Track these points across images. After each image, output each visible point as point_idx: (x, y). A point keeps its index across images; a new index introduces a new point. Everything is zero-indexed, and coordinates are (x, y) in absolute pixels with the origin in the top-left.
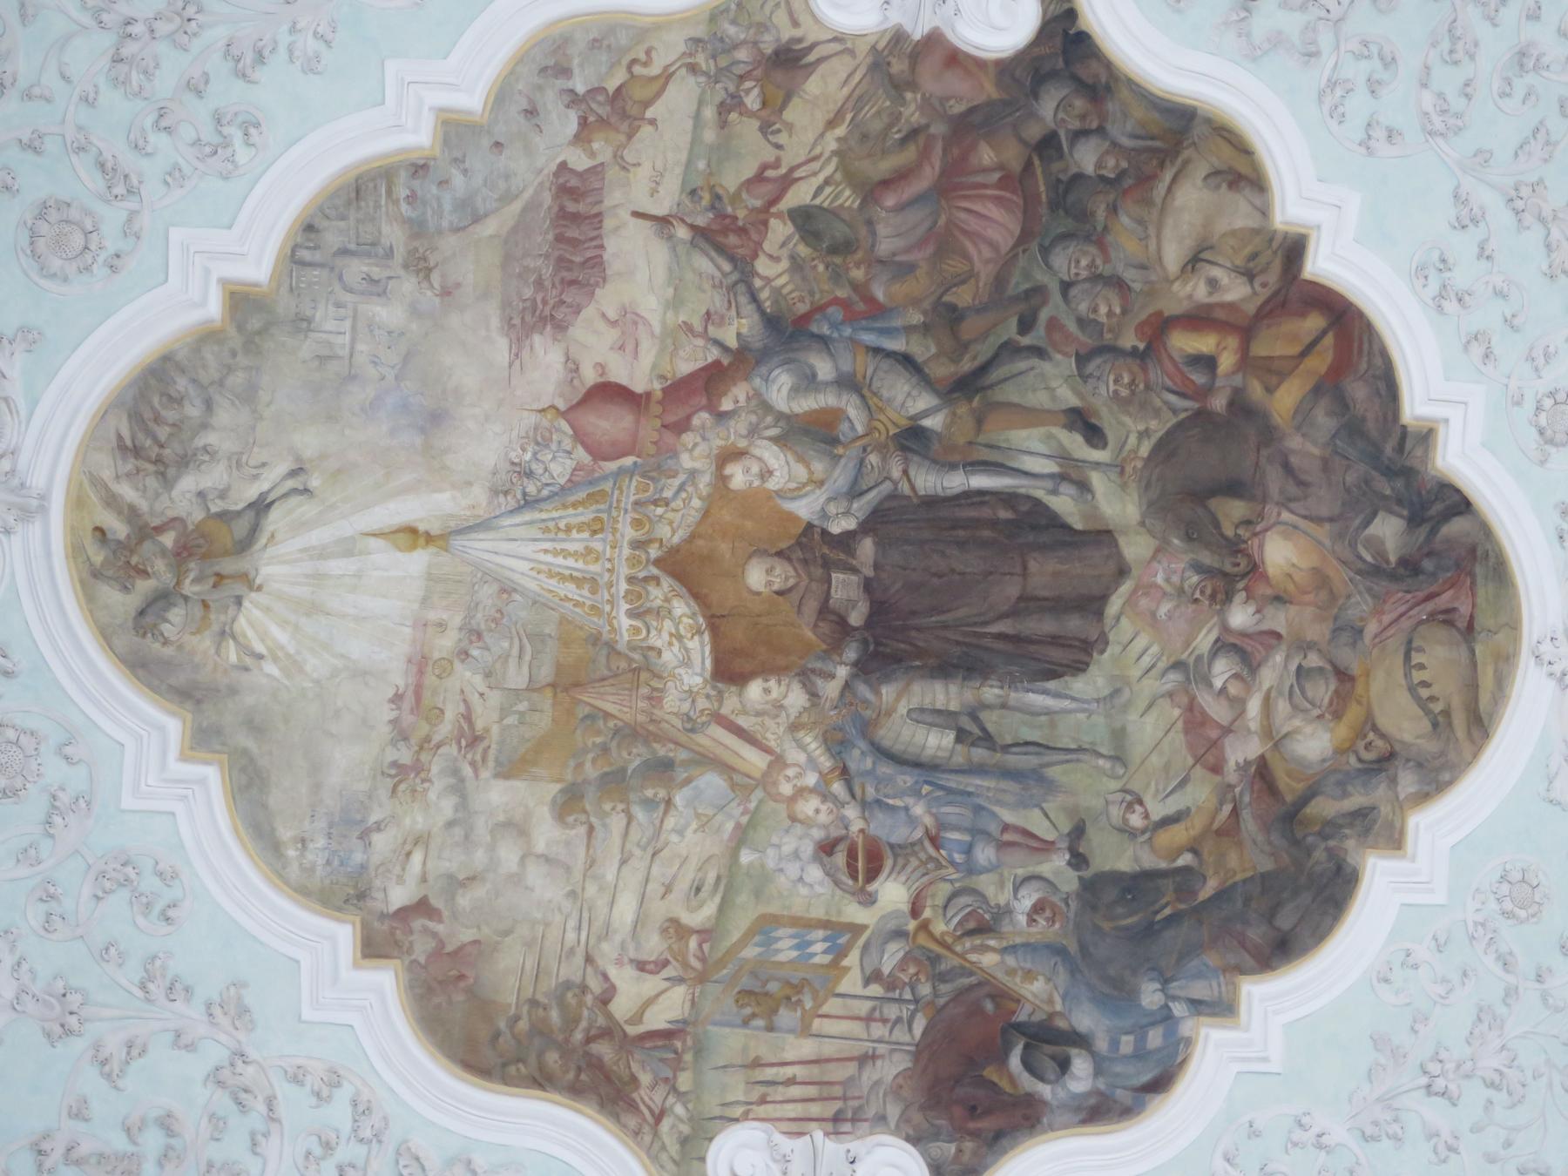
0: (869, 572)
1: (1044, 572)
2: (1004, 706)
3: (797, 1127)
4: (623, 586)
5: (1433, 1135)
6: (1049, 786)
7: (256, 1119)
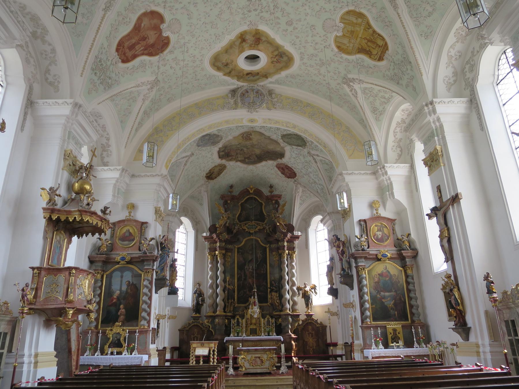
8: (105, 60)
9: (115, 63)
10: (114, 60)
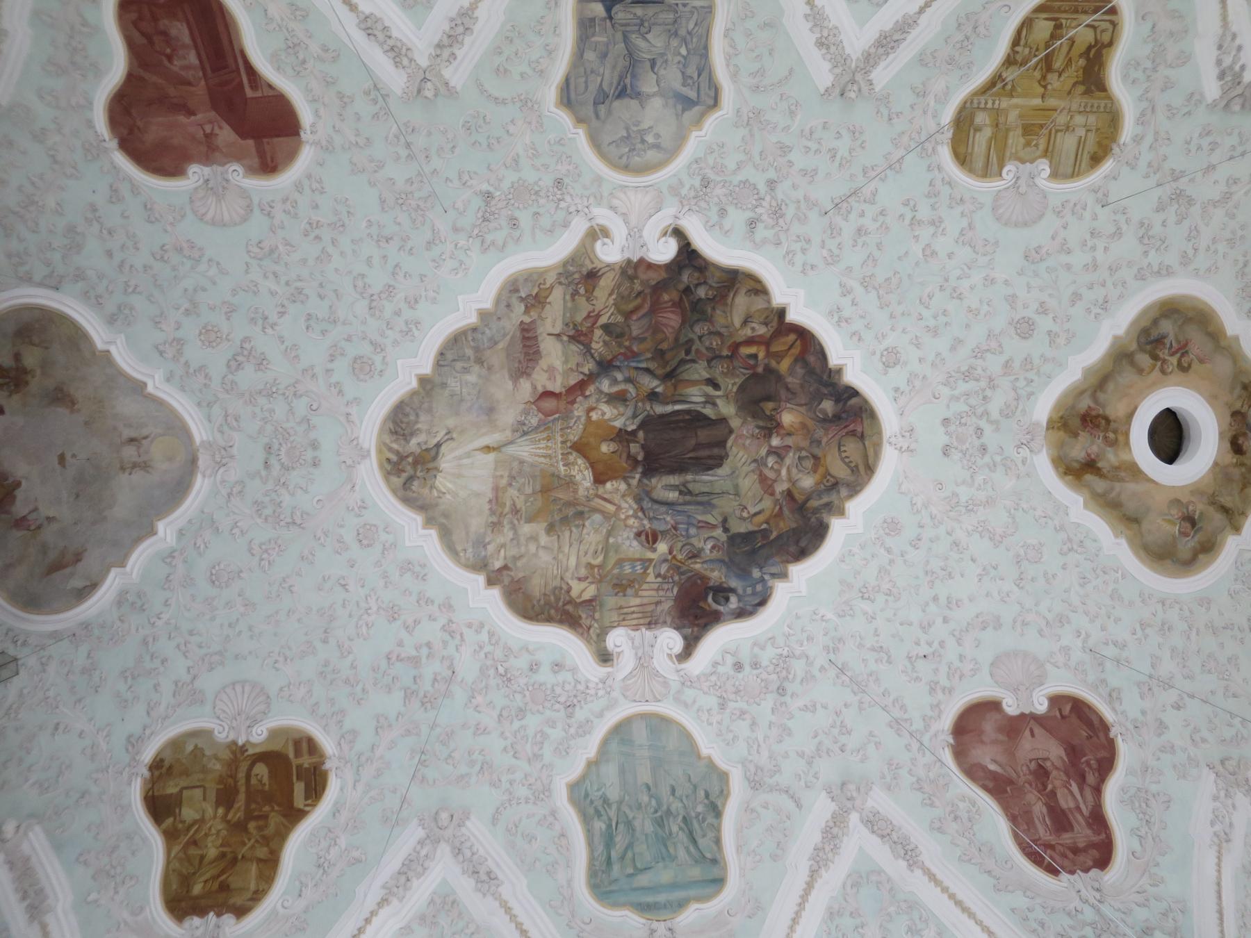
0: (643, 442)
1: (703, 435)
2: (695, 481)
3: (636, 628)
4: (560, 457)
5: (865, 613)
6: (714, 506)
7: (457, 641)
8: (1071, 922)
9: (1098, 895)
10: (1084, 892)
